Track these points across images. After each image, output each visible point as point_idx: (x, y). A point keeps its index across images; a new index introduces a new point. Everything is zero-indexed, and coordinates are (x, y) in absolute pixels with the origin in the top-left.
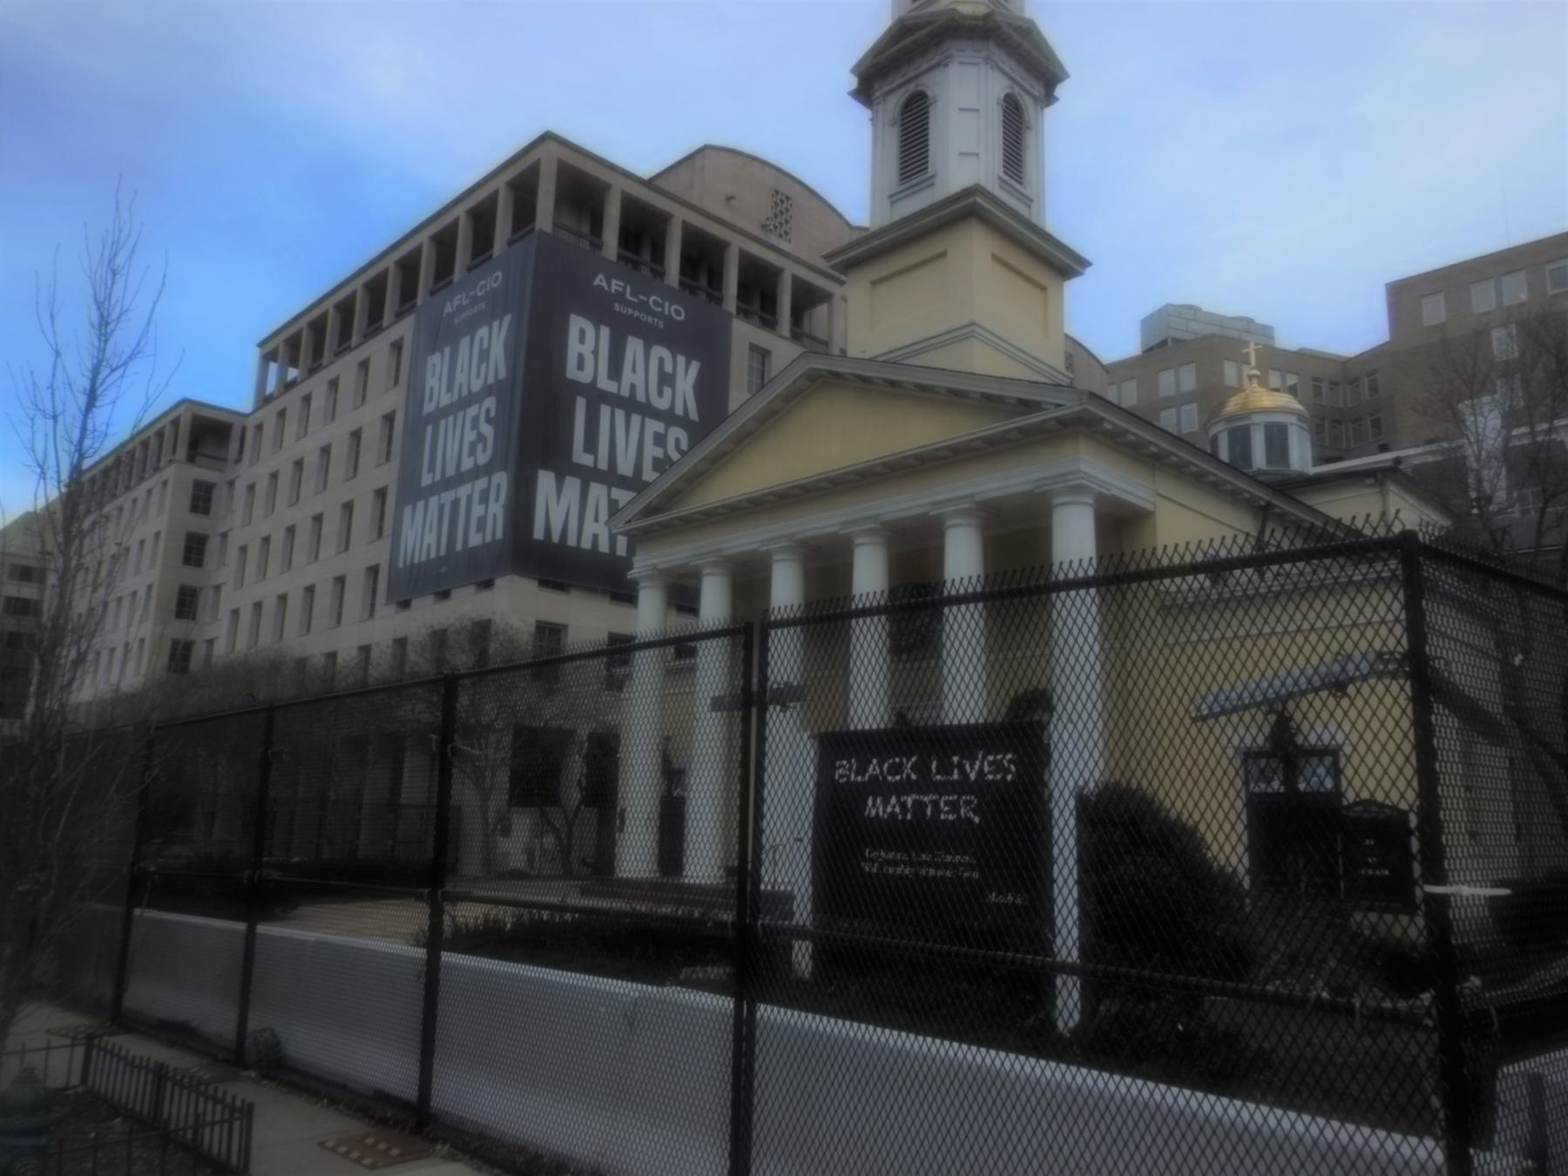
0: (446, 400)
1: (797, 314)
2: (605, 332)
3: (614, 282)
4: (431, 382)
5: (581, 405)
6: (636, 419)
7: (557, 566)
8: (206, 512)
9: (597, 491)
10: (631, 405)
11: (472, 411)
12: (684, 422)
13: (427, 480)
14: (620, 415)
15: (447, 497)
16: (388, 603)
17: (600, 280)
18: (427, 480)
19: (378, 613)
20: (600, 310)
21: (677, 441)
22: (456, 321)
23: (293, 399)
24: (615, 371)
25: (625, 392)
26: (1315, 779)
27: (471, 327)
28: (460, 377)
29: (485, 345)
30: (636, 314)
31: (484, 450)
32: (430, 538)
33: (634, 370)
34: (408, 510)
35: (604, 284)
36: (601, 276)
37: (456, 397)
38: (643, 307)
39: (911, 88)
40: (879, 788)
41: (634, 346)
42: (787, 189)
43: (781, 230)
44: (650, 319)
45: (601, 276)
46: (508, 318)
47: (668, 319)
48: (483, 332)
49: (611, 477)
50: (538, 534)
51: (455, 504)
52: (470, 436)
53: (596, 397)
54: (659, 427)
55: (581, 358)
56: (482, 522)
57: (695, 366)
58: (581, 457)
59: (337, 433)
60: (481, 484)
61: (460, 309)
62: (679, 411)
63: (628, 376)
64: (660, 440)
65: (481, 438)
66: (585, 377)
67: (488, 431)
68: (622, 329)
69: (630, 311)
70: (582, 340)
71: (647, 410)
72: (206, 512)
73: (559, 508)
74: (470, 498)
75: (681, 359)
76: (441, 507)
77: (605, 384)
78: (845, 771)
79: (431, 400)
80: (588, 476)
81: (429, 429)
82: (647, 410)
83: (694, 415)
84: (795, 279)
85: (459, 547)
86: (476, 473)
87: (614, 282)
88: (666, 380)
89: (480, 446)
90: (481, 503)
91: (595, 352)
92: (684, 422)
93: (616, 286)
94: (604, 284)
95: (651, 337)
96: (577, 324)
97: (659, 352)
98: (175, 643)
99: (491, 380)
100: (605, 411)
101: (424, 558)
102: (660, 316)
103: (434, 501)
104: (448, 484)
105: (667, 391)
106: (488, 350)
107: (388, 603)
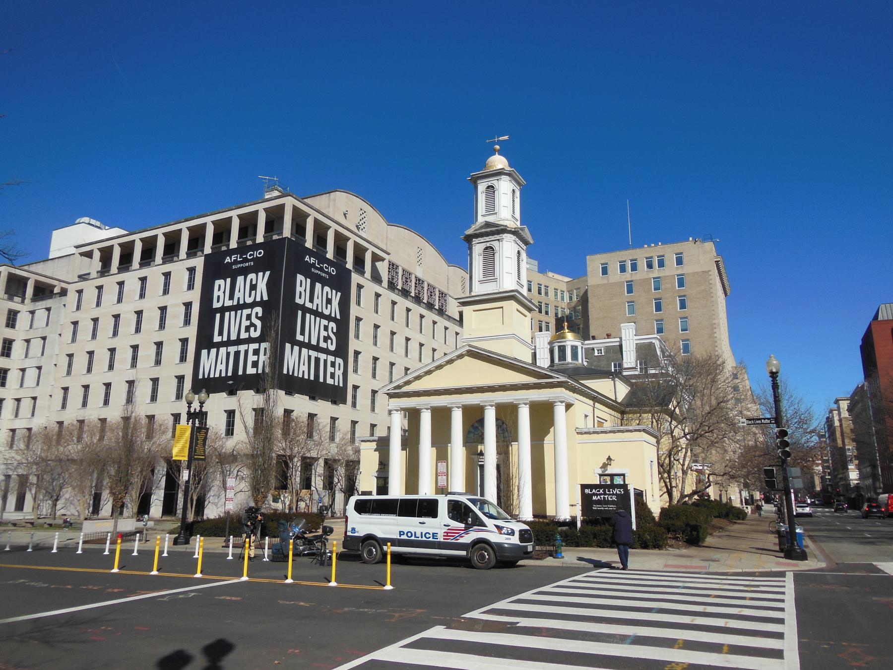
0: (228, 303)
2: (309, 281)
5: (300, 313)
6: (318, 319)
8: (13, 326)
11: (246, 312)
12: (334, 320)
13: (217, 339)
14: (313, 317)
15: (232, 349)
17: (307, 258)
18: (217, 339)
24: (311, 301)
27: (245, 272)
29: (254, 282)
31: (255, 331)
32: (221, 367)
34: (204, 352)
37: (235, 303)
38: (321, 269)
39: (488, 244)
40: (594, 494)
41: (318, 286)
43: (362, 227)
46: (268, 273)
48: (252, 276)
50: (285, 372)
51: (237, 354)
52: (245, 323)
53: (305, 310)
56: (255, 364)
57: (339, 294)
58: (299, 337)
62: (333, 315)
63: (316, 301)
67: (258, 323)
68: (315, 279)
71: (322, 316)
72: (13, 326)
74: (246, 352)
75: (334, 292)
76: (228, 354)
77: (308, 305)
78: (587, 491)
79: (218, 301)
80: (302, 345)
81: (218, 316)
82: (322, 316)
83: (338, 317)
84: (336, 232)
85: (240, 373)
86: (250, 340)
88: (329, 301)
89: (252, 329)
92: (334, 320)
93: (312, 260)
96: (300, 277)
97: (327, 289)
98: (232, 434)
100: (308, 315)
103: (223, 350)
104: (229, 343)
105: (329, 306)
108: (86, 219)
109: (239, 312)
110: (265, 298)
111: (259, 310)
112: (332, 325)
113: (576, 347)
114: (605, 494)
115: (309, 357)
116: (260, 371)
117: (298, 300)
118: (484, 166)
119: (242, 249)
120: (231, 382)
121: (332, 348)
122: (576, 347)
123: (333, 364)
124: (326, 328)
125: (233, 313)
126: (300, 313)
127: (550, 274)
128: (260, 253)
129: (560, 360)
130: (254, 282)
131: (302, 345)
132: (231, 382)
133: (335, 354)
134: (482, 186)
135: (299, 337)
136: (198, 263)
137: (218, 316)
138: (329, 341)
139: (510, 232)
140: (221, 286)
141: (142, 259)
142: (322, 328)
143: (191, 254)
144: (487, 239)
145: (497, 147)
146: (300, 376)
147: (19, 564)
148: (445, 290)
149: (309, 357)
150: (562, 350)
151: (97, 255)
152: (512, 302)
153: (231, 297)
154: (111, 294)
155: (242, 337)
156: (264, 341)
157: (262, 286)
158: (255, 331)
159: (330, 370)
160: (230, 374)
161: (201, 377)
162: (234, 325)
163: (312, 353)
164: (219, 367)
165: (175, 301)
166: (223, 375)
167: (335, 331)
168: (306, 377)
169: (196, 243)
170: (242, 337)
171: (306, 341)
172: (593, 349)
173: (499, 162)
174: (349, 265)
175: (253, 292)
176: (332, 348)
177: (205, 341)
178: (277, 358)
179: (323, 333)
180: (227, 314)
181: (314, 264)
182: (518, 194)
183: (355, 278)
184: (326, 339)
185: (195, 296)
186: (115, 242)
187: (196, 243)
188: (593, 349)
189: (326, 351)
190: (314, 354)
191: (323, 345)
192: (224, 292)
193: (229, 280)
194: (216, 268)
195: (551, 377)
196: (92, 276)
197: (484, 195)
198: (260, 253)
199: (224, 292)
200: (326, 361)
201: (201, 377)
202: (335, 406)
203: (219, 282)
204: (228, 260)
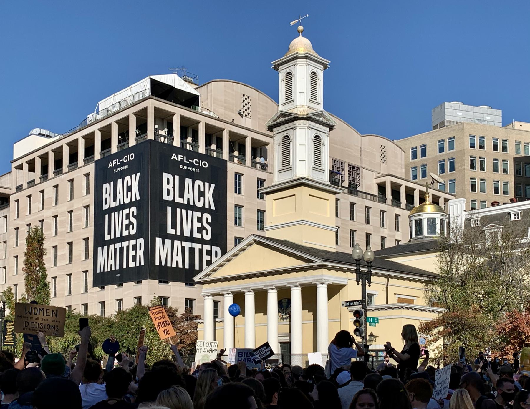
0: (113, 205)
1: (254, 154)
2: (177, 177)
3: (179, 156)
4: (105, 196)
5: (169, 209)
6: (190, 212)
7: (165, 274)
9: (177, 243)
10: (188, 207)
11: (126, 211)
12: (209, 211)
13: (107, 237)
14: (184, 211)
15: (118, 246)
16: (94, 286)
17: (174, 156)
18: (107, 237)
19: (89, 291)
21: (207, 219)
22: (115, 171)
23: (34, 191)
24: (181, 195)
25: (186, 202)
28: (119, 196)
29: (129, 184)
30: (189, 168)
31: (133, 228)
33: (188, 193)
34: (100, 249)
36: (174, 154)
38: (191, 165)
41: (188, 182)
44: (194, 170)
45: (174, 154)
46: (138, 174)
47: (201, 168)
48: (128, 178)
49: (182, 238)
50: (157, 263)
51: (121, 249)
52: (126, 222)
53: (174, 205)
54: (199, 214)
55: (168, 190)
57: (213, 186)
58: (170, 231)
59: (62, 209)
60: (133, 242)
61: (116, 167)
62: (207, 206)
63: (186, 195)
64: (200, 220)
65: (131, 223)
66: (170, 198)
67: (134, 221)
69: (186, 167)
70: (168, 183)
71: (194, 208)
73: (163, 251)
74: (128, 247)
75: (207, 184)
76: (115, 250)
77: (178, 200)
79: (106, 204)
80: (173, 238)
81: (107, 216)
82: (194, 208)
83: (213, 208)
85: (125, 267)
87: (179, 156)
88: (202, 194)
89: (131, 227)
90: (133, 250)
92: (209, 211)
93: (180, 157)
94: (176, 158)
95: (194, 177)
96: (166, 176)
97: (198, 183)
100: (178, 210)
102: (198, 167)
103: (112, 246)
104: (115, 241)
106: (131, 186)
107: (94, 286)
108: (37, 131)
110: (138, 198)
111: (134, 209)
112: (207, 216)
113: (434, 220)
115: (183, 248)
116: (138, 265)
117: (165, 197)
118: (287, 49)
119: (124, 151)
120: (119, 275)
121: (208, 237)
122: (434, 220)
123: (209, 253)
124: (200, 220)
125: (116, 213)
126: (169, 209)
129: (417, 234)
131: (173, 238)
132: (119, 275)
133: (211, 243)
134: (282, 75)
135: (170, 231)
136: (91, 168)
137: (107, 216)
138: (204, 232)
139: (302, 118)
141: (70, 163)
142: (195, 220)
144: (283, 128)
145: (301, 28)
146: (174, 265)
148: (357, 164)
149: (183, 248)
150: (419, 223)
151: (26, 167)
152: (303, 187)
153: (115, 200)
154: (36, 205)
155: (124, 235)
157: (135, 187)
158: (133, 228)
159: (206, 258)
160: (118, 268)
163: (184, 244)
164: (175, 258)
165: (78, 205)
166: (113, 269)
167: (209, 221)
168: (180, 266)
169: (89, 151)
170: (124, 235)
171: (179, 233)
172: (509, 213)
173: (301, 44)
175: (129, 193)
176: (208, 237)
177: (100, 241)
178: (150, 251)
179: (197, 225)
180: (113, 214)
181: (182, 161)
182: (320, 75)
183: (232, 168)
184: (200, 230)
185: (90, 200)
186: (48, 149)
187: (89, 151)
188: (509, 213)
189: (202, 241)
190: (187, 245)
191: (197, 235)
192: (110, 195)
193: (112, 183)
194: (104, 175)
195: (312, 261)
196: (36, 183)
197: (284, 82)
198: (131, 157)
199: (110, 195)
200: (201, 251)
201: (98, 272)
203: (106, 186)
204: (110, 165)
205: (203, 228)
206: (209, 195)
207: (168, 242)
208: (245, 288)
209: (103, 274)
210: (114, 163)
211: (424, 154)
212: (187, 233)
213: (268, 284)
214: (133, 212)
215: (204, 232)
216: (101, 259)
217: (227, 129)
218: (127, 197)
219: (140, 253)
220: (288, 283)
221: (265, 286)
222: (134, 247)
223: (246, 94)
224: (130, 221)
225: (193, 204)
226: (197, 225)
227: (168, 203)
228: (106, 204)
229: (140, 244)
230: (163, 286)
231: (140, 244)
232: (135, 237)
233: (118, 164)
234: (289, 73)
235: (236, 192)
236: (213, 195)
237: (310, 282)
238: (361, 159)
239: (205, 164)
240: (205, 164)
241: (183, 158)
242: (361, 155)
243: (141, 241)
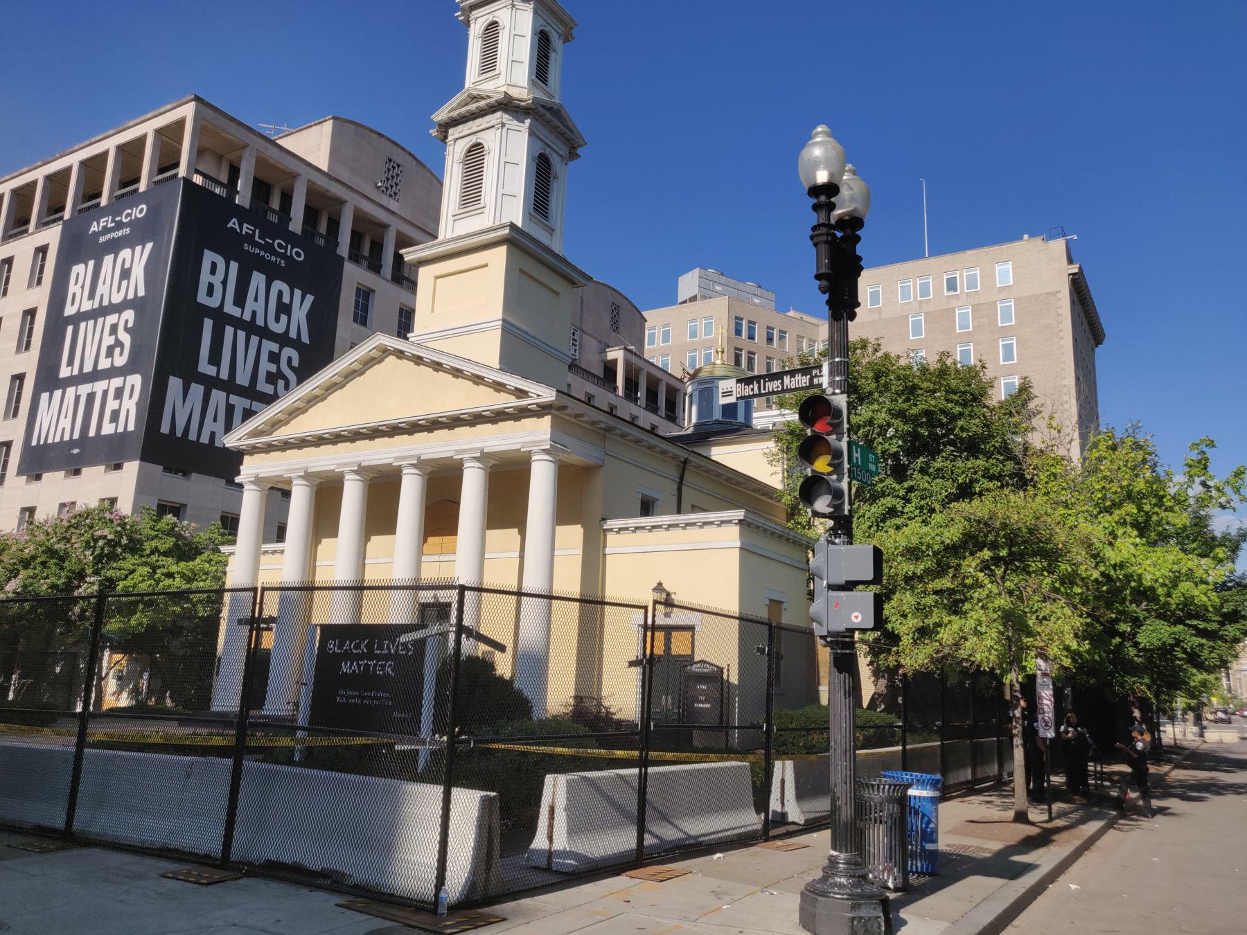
0: (87, 306)
2: (234, 266)
4: (73, 288)
5: (208, 324)
6: (254, 340)
9: (218, 396)
10: (251, 328)
11: (112, 319)
14: (241, 335)
15: (84, 390)
16: (20, 472)
17: (233, 223)
18: (65, 372)
20: (230, 247)
21: (290, 359)
24: (240, 301)
25: (247, 317)
26: (680, 646)
27: (114, 247)
28: (102, 289)
29: (127, 266)
30: (262, 253)
31: (121, 354)
32: (66, 423)
33: (256, 300)
34: (45, 396)
35: (237, 227)
36: (234, 220)
37: (96, 306)
38: (269, 248)
41: (258, 279)
42: (399, 157)
44: (273, 259)
46: (149, 246)
47: (289, 259)
48: (125, 253)
51: (91, 396)
52: (109, 340)
54: (275, 347)
57: (310, 299)
58: (205, 368)
60: (117, 382)
61: (106, 230)
62: (293, 334)
64: (274, 358)
65: (119, 343)
66: (214, 302)
67: (126, 339)
69: (257, 251)
70: (213, 271)
71: (265, 333)
74: (105, 393)
75: (298, 293)
76: (77, 398)
77: (231, 309)
78: (332, 646)
79: (73, 304)
80: (211, 383)
81: (70, 329)
82: (265, 333)
83: (305, 339)
85: (92, 433)
88: (284, 309)
89: (117, 350)
91: (224, 283)
92: (296, 344)
94: (237, 227)
95: (272, 274)
96: (209, 257)
97: (279, 285)
99: (131, 296)
100: (229, 330)
101: (57, 440)
102: (283, 256)
103: (71, 391)
104: (82, 378)
105: (284, 318)
106: (130, 269)
107: (20, 472)
109: (100, 320)
110: (141, 293)
111: (129, 315)
112: (288, 352)
114: (370, 655)
117: (202, 298)
120: (76, 451)
124: (274, 358)
125: (91, 323)
126: (208, 324)
127: (792, 313)
128: (141, 211)
130: (127, 266)
131: (211, 383)
132: (76, 451)
135: (205, 368)
136: (52, 236)
137: (70, 329)
138: (281, 383)
140: (80, 272)
143: (42, 224)
146: (205, 439)
147: (709, 770)
155: (100, 367)
156: (132, 372)
157: (138, 273)
158: (121, 354)
160: (76, 436)
161: (34, 443)
162: (97, 344)
163: (234, 399)
167: (295, 363)
170: (100, 367)
171: (224, 375)
174: (344, 249)
177: (48, 379)
179: (266, 366)
185: (40, 298)
192: (83, 287)
193: (91, 263)
199: (83, 287)
201: (34, 443)
202: (75, 480)
203: (78, 269)
204: (94, 228)
205: (280, 375)
206: (300, 313)
207: (197, 390)
208: (345, 464)
209: (45, 448)
210: (102, 224)
211: (666, 337)
212: (243, 379)
213: (406, 454)
214: (127, 322)
215: (281, 383)
216: (45, 416)
217: (353, 202)
218: (119, 290)
219: (130, 405)
220: (459, 452)
221: (397, 458)
222: (119, 393)
223: (394, 158)
224: (117, 340)
225: (262, 325)
226: (266, 366)
227: (206, 311)
228: (73, 304)
229: (133, 386)
230: (175, 480)
231: (133, 386)
232: (123, 372)
233: (110, 225)
234: (494, 24)
235: (355, 320)
236: (310, 316)
237: (517, 447)
238: (581, 317)
239: (298, 254)
240: (298, 254)
241: (254, 232)
242: (582, 310)
243: (136, 380)
